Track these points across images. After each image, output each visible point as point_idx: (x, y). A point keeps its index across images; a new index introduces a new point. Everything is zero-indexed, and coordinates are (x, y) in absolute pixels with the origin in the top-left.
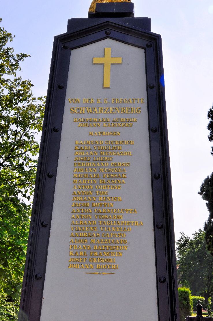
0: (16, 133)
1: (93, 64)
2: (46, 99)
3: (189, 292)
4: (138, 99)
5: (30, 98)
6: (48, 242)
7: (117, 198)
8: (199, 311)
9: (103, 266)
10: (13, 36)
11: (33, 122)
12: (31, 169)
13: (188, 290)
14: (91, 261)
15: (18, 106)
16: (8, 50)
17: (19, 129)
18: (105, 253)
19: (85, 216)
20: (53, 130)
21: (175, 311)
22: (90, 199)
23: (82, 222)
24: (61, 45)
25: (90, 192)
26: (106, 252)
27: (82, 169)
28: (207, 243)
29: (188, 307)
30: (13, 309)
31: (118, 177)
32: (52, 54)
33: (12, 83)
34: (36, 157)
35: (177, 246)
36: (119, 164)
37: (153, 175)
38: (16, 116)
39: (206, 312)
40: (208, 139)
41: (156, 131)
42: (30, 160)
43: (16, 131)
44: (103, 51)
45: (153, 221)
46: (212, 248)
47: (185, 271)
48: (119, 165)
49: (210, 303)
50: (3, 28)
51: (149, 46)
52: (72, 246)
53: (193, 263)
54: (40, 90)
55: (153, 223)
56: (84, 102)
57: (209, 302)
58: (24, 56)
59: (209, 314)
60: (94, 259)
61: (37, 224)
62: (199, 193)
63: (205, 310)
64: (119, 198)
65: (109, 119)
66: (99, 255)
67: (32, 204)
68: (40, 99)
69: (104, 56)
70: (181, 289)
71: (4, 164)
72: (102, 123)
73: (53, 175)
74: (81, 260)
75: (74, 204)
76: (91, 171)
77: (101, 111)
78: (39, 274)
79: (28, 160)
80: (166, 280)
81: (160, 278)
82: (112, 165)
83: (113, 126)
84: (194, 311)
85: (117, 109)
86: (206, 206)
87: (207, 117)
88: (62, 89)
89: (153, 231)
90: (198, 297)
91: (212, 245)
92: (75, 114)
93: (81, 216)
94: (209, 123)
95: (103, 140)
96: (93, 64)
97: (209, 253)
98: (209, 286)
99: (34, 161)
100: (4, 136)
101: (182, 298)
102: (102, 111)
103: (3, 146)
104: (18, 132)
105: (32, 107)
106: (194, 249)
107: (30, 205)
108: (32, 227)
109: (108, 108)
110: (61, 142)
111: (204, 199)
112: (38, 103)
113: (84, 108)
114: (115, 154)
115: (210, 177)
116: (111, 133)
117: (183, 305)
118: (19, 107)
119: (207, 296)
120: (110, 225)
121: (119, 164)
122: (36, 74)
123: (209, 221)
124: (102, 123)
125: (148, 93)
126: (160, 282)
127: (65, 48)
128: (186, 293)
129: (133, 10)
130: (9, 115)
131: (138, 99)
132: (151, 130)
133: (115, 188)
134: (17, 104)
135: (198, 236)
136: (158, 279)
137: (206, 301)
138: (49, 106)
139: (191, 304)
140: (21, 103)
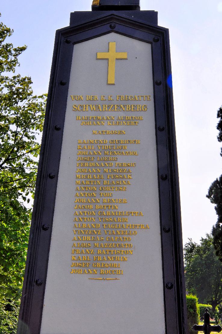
0: (16, 134)
1: (97, 59)
2: (47, 97)
3: (196, 300)
4: (145, 97)
5: (31, 97)
6: (48, 260)
7: (122, 200)
8: (206, 318)
9: (108, 271)
10: (11, 30)
11: (34, 122)
12: (31, 171)
13: (195, 298)
14: (94, 266)
15: (18, 105)
16: (8, 46)
17: (19, 129)
18: (109, 257)
19: (88, 218)
20: (55, 129)
21: (183, 314)
22: (94, 201)
23: (85, 225)
24: (63, 39)
25: (94, 193)
26: (110, 257)
27: (85, 169)
28: (216, 248)
29: (195, 315)
30: (12, 321)
31: (123, 177)
32: (52, 60)
33: (11, 81)
34: (37, 159)
35: (184, 252)
36: (124, 164)
37: (160, 176)
38: (16, 115)
39: (214, 321)
40: (217, 140)
41: (163, 129)
42: (31, 161)
43: (16, 131)
44: (107, 45)
45: (159, 225)
46: (220, 253)
47: (192, 278)
48: (124, 166)
49: (218, 311)
50: (2, 23)
51: (156, 41)
52: (74, 250)
53: (200, 270)
54: (41, 87)
55: (160, 226)
56: (87, 99)
57: (216, 310)
58: (23, 49)
59: (217, 323)
60: (98, 264)
61: (38, 227)
62: (207, 196)
63: (212, 318)
64: (124, 199)
65: (114, 117)
66: (103, 260)
67: (32, 207)
68: (41, 97)
69: (108, 51)
70: (189, 296)
71: (3, 166)
72: (106, 121)
73: (55, 176)
74: (84, 264)
75: (76, 206)
76: (95, 172)
77: (105, 108)
78: (40, 280)
79: (29, 162)
80: (174, 287)
81: (167, 284)
82: (116, 165)
83: (117, 124)
84: (201, 319)
85: (122, 106)
86: (214, 210)
87: (216, 116)
88: (64, 85)
89: (160, 235)
90: (206, 305)
91: (221, 250)
92: (77, 112)
93: (84, 194)
94: (218, 122)
95: (108, 139)
96: (97, 59)
97: (217, 258)
98: (217, 293)
99: (35, 163)
100: (3, 137)
101: (188, 306)
102: (106, 108)
103: (2, 147)
104: (18, 132)
105: (34, 107)
106: (201, 255)
107: (31, 209)
108: (32, 231)
109: (112, 105)
110: (63, 142)
111: (212, 202)
112: (40, 100)
113: (87, 106)
114: (120, 154)
115: (219, 179)
116: (115, 132)
117: (190, 313)
118: (20, 106)
119: (214, 304)
120: (115, 228)
121: (124, 164)
122: (36, 68)
123: (218, 225)
124: (106, 121)
125: (155, 95)
126: (168, 289)
127: (68, 42)
128: (193, 300)
129: (139, 3)
130: (9, 115)
131: (145, 97)
132: (157, 129)
133: (120, 190)
134: (17, 103)
135: (205, 242)
136: (165, 284)
137: (214, 309)
138: (50, 103)
139: (198, 313)
140: (21, 101)
